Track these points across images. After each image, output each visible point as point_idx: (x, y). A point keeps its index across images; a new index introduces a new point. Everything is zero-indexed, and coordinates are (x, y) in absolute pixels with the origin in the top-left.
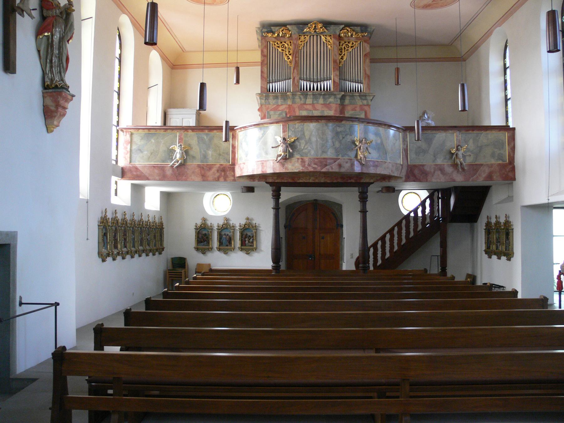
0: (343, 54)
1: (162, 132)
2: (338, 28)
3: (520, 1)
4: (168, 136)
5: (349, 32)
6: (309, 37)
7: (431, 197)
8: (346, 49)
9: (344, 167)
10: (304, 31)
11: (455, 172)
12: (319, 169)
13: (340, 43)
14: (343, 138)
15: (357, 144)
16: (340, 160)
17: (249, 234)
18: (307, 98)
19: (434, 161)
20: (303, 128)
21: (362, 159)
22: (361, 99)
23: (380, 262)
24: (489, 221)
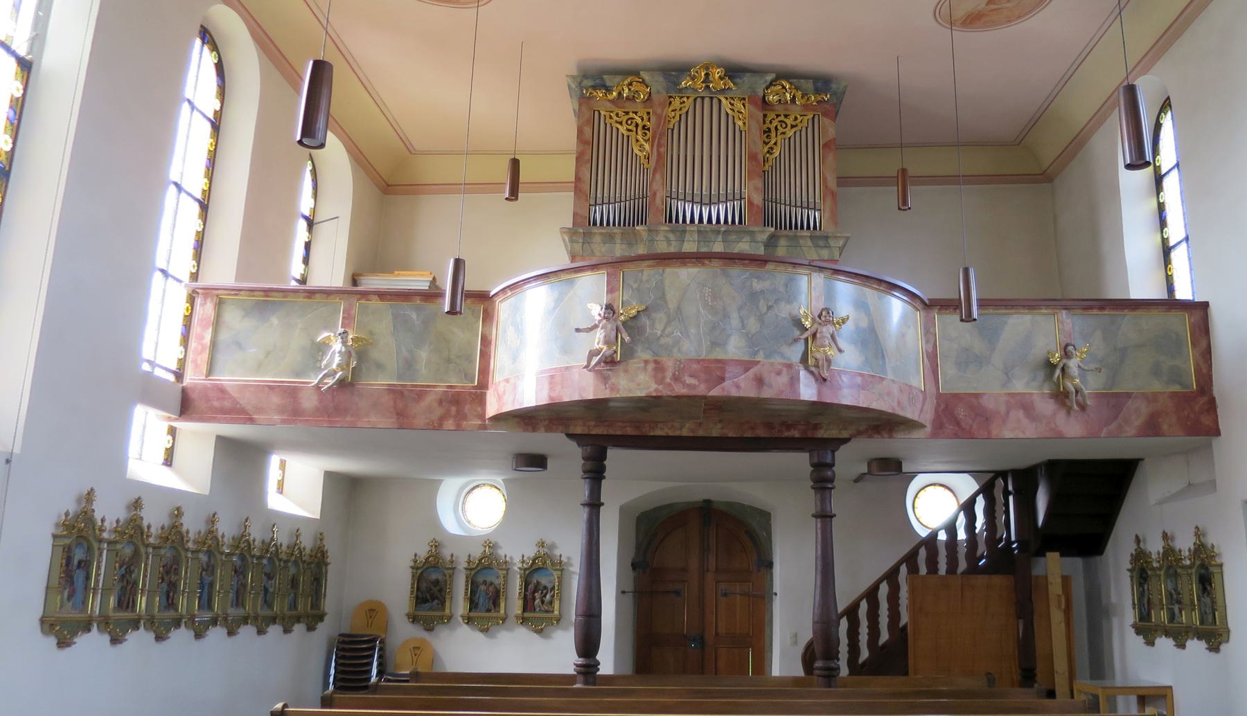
0: (773, 142)
1: (301, 299)
2: (762, 82)
3: (1194, 3)
4: (316, 310)
5: (786, 90)
6: (691, 100)
7: (986, 490)
8: (781, 130)
9: (770, 386)
10: (681, 87)
11: (1061, 415)
12: (701, 390)
13: (765, 116)
14: (769, 308)
15: (807, 324)
16: (759, 366)
17: (544, 581)
18: (683, 241)
19: (1004, 386)
20: (662, 281)
21: (820, 363)
22: (817, 246)
23: (865, 654)
24: (1140, 548)
